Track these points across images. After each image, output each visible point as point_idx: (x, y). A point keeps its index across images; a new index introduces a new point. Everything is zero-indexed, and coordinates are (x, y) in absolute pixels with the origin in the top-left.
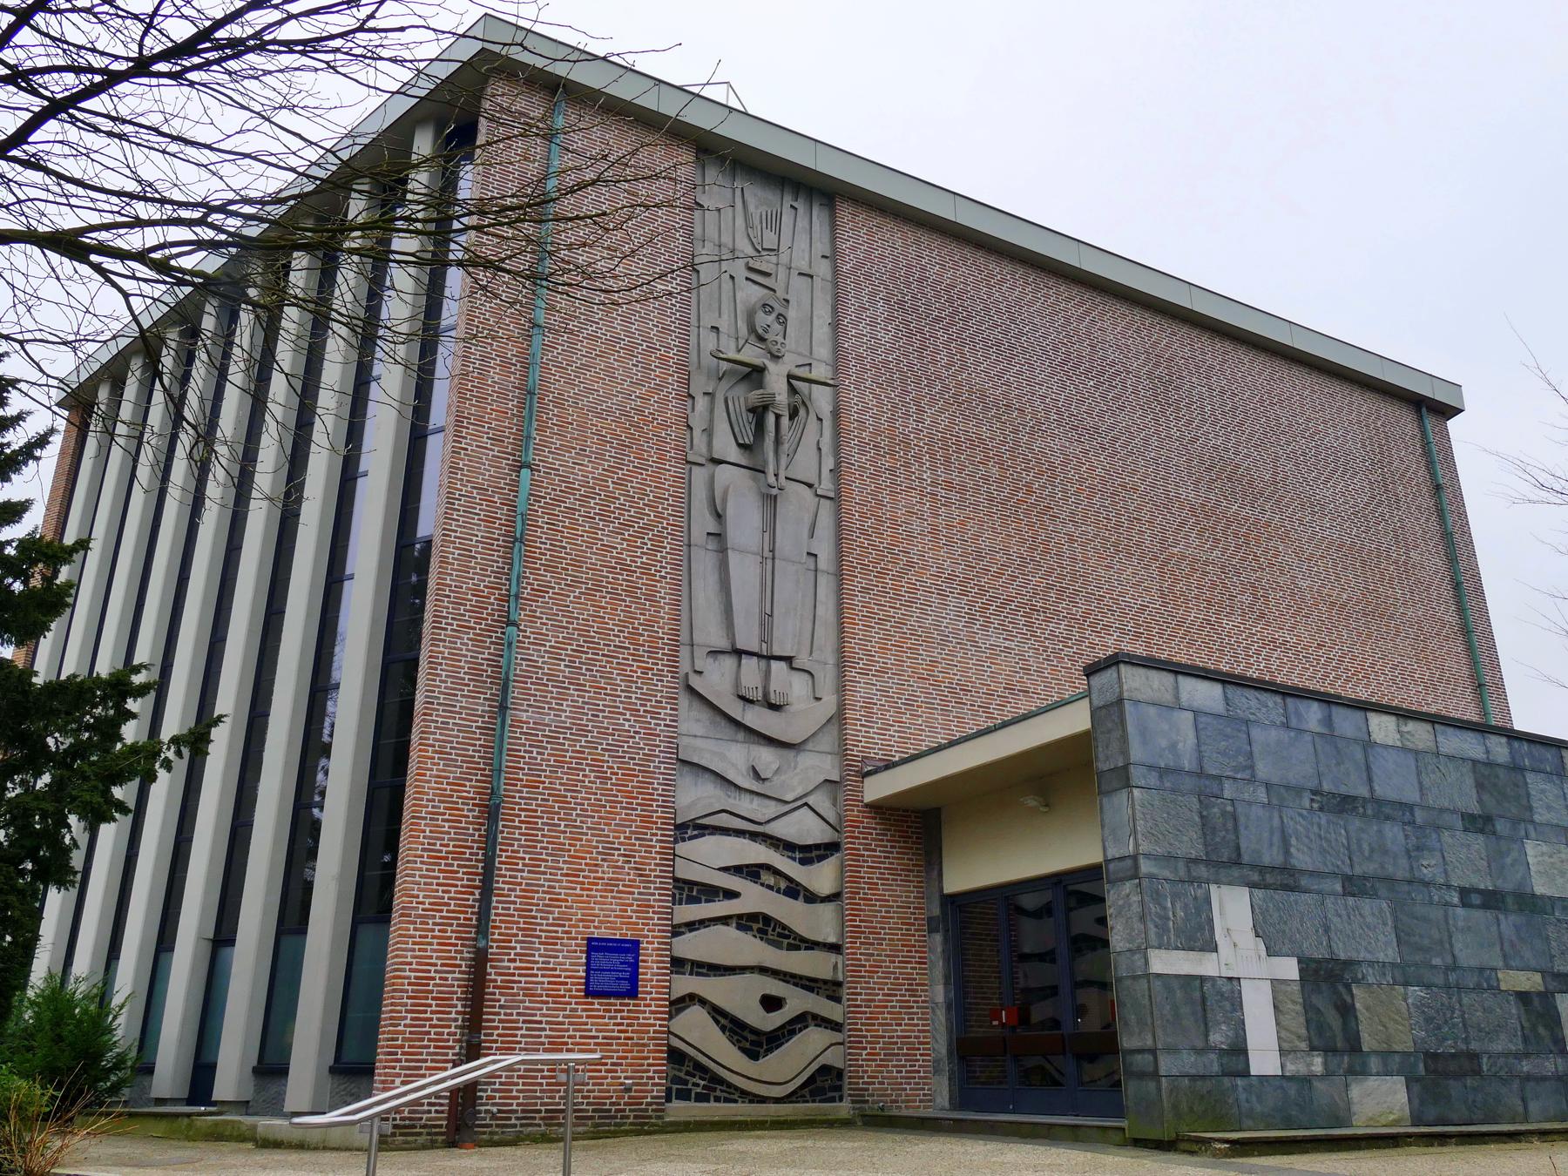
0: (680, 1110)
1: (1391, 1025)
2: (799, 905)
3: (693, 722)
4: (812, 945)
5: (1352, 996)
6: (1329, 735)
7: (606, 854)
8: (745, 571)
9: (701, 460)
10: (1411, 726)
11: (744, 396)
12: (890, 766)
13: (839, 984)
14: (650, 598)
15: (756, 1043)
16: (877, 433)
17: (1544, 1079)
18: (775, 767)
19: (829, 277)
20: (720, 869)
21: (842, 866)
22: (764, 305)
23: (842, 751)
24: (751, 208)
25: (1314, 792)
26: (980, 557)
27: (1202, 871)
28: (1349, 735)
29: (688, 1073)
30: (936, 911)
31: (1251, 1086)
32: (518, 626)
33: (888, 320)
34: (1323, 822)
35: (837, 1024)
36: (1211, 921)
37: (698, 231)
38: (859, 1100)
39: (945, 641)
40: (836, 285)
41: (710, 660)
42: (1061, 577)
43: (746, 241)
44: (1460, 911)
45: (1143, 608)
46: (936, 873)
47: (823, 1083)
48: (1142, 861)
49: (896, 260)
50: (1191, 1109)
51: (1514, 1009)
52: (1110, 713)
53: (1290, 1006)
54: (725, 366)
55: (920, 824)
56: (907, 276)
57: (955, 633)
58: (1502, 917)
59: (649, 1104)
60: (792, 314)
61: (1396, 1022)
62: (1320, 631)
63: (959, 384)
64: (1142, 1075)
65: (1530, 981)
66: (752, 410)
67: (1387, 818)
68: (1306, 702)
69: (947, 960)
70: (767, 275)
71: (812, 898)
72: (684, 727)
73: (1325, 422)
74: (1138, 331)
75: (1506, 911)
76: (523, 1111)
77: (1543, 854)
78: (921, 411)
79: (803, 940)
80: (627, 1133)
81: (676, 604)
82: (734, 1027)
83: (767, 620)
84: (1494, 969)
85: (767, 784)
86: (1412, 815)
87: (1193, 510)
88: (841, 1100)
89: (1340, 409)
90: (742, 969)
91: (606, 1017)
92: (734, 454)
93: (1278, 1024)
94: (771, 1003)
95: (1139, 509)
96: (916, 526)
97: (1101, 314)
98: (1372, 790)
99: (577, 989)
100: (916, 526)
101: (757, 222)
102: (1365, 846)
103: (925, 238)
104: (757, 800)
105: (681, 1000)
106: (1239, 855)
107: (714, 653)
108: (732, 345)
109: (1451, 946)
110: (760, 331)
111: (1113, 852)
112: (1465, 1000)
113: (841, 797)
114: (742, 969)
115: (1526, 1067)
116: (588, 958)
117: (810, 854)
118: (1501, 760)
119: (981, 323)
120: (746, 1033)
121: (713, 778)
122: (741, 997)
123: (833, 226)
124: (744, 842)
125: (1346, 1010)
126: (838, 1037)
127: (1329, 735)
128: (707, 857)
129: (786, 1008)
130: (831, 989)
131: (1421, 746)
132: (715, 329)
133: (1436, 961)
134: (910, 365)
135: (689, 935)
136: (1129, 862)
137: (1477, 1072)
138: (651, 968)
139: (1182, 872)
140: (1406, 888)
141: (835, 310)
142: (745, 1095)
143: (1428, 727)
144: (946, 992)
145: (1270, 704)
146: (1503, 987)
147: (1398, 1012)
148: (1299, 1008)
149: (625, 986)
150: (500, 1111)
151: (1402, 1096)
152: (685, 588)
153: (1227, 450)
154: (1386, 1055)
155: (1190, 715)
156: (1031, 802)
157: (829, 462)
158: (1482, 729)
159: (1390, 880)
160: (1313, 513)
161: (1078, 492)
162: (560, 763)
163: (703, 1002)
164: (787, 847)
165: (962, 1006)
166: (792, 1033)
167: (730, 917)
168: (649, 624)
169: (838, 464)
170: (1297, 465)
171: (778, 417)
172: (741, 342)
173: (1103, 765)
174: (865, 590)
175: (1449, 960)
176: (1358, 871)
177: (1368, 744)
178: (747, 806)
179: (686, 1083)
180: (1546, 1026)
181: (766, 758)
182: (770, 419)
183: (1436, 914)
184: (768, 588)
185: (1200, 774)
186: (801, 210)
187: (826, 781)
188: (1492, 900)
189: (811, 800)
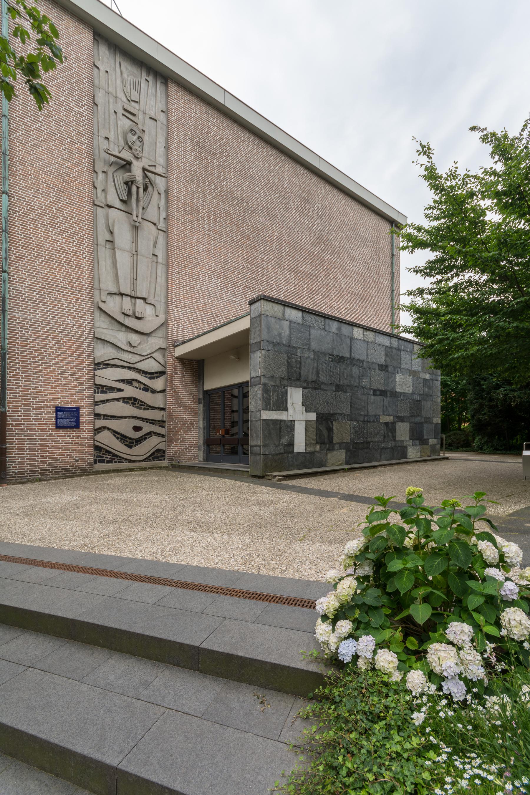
0: (99, 466)
1: (344, 434)
2: (149, 394)
3: (102, 323)
4: (154, 408)
5: (333, 425)
6: (339, 334)
7: (63, 374)
8: (123, 259)
9: (102, 205)
10: (368, 333)
11: (121, 177)
12: (183, 343)
13: (164, 422)
14: (78, 266)
15: (131, 443)
16: (185, 204)
17: (388, 448)
18: (138, 342)
19: (165, 123)
20: (115, 381)
21: (166, 380)
22: (132, 130)
23: (167, 337)
24: (125, 75)
25: (330, 355)
26: (226, 264)
27: (286, 382)
28: (346, 334)
29: (103, 454)
30: (201, 396)
31: (294, 456)
32: (8, 273)
33: (192, 150)
34: (332, 366)
35: (163, 435)
36: (286, 400)
37: (96, 82)
38: (171, 459)
39: (210, 297)
40: (168, 127)
41: (109, 297)
42: (258, 275)
43: (123, 94)
44: (372, 397)
45: (287, 290)
46: (201, 383)
47: (158, 454)
48: (262, 378)
49: (196, 120)
50: (271, 465)
51: (383, 428)
52: (256, 320)
53: (311, 429)
54: (113, 159)
55: (195, 366)
56: (202, 129)
57: (215, 294)
58: (385, 399)
59: (86, 465)
60: (146, 138)
61: (346, 433)
62: (346, 304)
63: (222, 187)
64: (255, 454)
65: (389, 419)
66: (126, 183)
67: (354, 365)
68: (333, 321)
69: (204, 413)
70: (134, 115)
71: (154, 391)
72: (97, 324)
73: (360, 225)
74: (297, 175)
75: (386, 397)
76: (30, 471)
77: (401, 378)
78: (205, 197)
79: (150, 406)
80: (77, 476)
81: (92, 270)
82: (122, 438)
83: (134, 281)
84: (379, 415)
85: (135, 348)
86: (363, 364)
87: (309, 254)
88: (164, 459)
89: (366, 221)
90: (126, 417)
91: (65, 437)
92: (118, 204)
93: (306, 435)
94: (137, 429)
95: (290, 251)
96: (201, 248)
97: (284, 165)
98: (351, 354)
99: (52, 425)
100: (201, 248)
101: (128, 85)
102: (345, 375)
103: (211, 111)
104: (131, 355)
105: (100, 428)
106: (300, 377)
107: (111, 294)
108: (116, 149)
109: (368, 408)
110: (130, 144)
111: (253, 375)
112: (369, 425)
113: (166, 354)
114: (126, 417)
115: (383, 445)
116: (56, 415)
117: (153, 375)
118: (394, 346)
119: (233, 159)
120: (127, 439)
121: (111, 345)
122: (125, 427)
123: (167, 96)
124: (126, 370)
125: (330, 430)
126: (164, 439)
127: (339, 334)
128: (108, 376)
129: (143, 430)
130: (161, 423)
131: (370, 340)
132: (106, 138)
133: (362, 413)
134: (201, 174)
135: (102, 405)
136: (258, 379)
137: (368, 448)
138: (85, 417)
139: (278, 382)
140: (356, 389)
141: (167, 141)
142: (126, 460)
143: (373, 333)
144: (203, 423)
145: (319, 321)
146: (381, 421)
147: (347, 430)
148: (314, 430)
149: (74, 424)
150: (18, 472)
151: (344, 456)
152: (96, 264)
153: (324, 231)
154: (340, 444)
155: (288, 323)
156: (232, 357)
157: (163, 215)
158: (390, 335)
159: (351, 386)
160: (351, 260)
161: (267, 242)
162: (37, 337)
163: (109, 429)
164: (145, 373)
165: (208, 428)
166: (146, 439)
167: (120, 398)
168: (78, 279)
169: (167, 216)
170: (348, 241)
171: (138, 188)
172: (121, 148)
173: (252, 341)
174: (178, 273)
175: (366, 413)
176: (341, 383)
177: (352, 338)
178: (126, 357)
179: (103, 457)
180: (391, 433)
181: (135, 338)
182: (134, 189)
183: (364, 398)
184: (134, 267)
185: (289, 346)
186: (151, 82)
187: (160, 348)
188: (383, 393)
189: (154, 355)
